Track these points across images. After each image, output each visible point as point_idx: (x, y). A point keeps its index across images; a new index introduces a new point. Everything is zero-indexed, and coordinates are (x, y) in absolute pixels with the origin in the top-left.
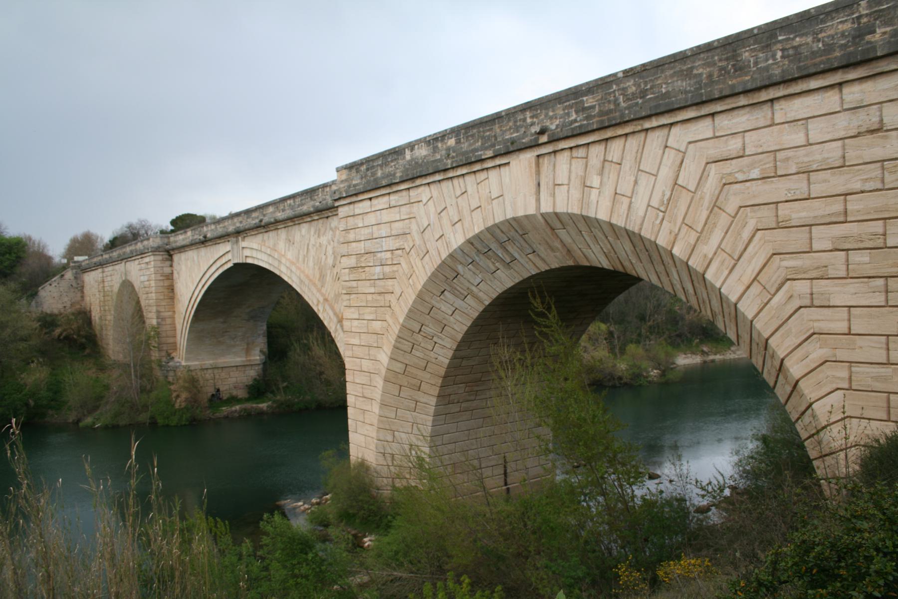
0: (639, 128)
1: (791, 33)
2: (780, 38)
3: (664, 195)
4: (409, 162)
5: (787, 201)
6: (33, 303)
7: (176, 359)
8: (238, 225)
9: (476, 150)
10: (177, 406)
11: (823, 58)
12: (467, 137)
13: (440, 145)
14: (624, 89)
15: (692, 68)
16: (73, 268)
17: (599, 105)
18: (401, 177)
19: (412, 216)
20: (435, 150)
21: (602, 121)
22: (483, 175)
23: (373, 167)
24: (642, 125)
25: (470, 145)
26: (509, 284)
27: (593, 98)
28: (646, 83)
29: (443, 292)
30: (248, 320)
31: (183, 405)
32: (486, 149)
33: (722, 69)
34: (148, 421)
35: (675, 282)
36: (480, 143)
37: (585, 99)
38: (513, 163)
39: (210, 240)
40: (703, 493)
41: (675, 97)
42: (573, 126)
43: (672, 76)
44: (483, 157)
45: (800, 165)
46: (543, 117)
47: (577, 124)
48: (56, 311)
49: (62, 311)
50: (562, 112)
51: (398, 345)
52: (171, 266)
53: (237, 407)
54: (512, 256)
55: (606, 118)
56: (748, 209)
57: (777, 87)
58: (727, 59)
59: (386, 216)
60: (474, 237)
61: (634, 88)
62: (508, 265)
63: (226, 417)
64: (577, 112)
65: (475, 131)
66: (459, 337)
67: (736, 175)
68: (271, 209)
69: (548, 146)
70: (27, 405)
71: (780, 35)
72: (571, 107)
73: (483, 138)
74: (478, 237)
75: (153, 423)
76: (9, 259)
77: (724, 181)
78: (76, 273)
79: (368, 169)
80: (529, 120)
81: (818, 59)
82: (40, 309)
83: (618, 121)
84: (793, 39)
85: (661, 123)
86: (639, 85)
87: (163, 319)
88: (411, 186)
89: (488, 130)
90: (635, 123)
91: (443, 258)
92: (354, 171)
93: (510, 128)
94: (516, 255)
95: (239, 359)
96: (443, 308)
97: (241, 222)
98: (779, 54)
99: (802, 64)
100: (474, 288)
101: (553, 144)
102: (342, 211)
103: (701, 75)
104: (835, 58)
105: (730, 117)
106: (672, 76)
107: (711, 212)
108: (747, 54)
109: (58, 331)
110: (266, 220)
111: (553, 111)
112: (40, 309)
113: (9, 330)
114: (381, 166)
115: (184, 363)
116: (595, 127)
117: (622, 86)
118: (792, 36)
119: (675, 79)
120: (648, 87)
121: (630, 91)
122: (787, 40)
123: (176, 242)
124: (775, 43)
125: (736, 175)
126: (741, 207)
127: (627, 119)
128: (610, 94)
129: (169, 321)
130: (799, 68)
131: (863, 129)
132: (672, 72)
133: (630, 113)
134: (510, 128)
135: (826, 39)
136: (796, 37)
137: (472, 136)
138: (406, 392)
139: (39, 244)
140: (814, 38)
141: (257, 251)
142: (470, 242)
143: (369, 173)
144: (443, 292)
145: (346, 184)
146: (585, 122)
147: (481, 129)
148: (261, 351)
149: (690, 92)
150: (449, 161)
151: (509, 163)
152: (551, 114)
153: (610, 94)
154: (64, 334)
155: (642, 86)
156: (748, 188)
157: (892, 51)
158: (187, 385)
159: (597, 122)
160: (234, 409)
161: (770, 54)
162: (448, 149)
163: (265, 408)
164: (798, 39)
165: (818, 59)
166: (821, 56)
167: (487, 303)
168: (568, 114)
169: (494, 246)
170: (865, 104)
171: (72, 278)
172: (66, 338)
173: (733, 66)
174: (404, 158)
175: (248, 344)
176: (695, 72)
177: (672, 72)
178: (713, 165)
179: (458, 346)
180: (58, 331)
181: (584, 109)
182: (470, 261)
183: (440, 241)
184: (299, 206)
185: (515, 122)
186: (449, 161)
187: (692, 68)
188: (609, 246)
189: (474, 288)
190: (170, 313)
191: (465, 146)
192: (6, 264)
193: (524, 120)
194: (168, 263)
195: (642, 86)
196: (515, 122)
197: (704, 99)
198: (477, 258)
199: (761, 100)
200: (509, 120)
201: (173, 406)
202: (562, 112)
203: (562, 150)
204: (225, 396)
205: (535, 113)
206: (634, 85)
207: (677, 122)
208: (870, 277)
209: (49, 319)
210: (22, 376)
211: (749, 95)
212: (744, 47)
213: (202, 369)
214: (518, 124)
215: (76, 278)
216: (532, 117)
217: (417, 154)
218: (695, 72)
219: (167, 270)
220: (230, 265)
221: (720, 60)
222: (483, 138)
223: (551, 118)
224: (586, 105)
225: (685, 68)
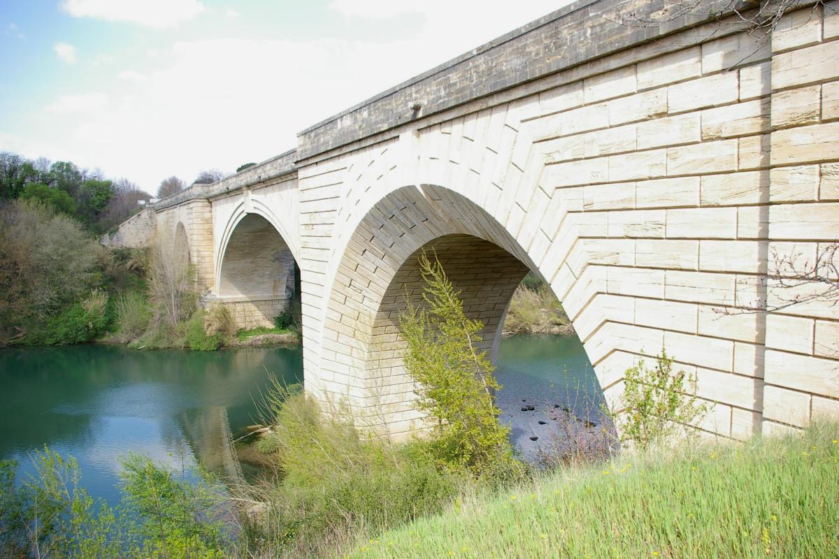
1: (600, 10)
2: (591, 15)
5: (592, 185)
6: (115, 238)
7: (213, 293)
8: (249, 179)
10: (208, 333)
11: (618, 36)
14: (476, 67)
15: (525, 46)
16: (150, 208)
18: (332, 145)
25: (377, 117)
29: (365, 251)
30: (274, 261)
31: (214, 333)
33: (547, 47)
34: (183, 345)
37: (451, 75)
38: (401, 136)
39: (232, 191)
41: (508, 75)
42: (439, 102)
43: (511, 54)
45: (602, 148)
47: (441, 101)
48: (133, 246)
49: (139, 245)
50: (435, 88)
51: (333, 296)
52: (211, 212)
53: (261, 337)
54: (412, 223)
55: (460, 95)
57: (585, 66)
58: (551, 37)
63: (251, 345)
65: (380, 104)
66: (383, 292)
67: (554, 155)
68: (269, 167)
69: (424, 120)
70: (87, 326)
71: (591, 12)
73: (384, 111)
75: (187, 348)
76: (99, 199)
78: (151, 213)
81: (614, 38)
82: (120, 243)
84: (601, 16)
85: (500, 102)
87: (203, 257)
88: (340, 153)
92: (307, 136)
95: (267, 295)
96: (367, 266)
97: (251, 177)
98: (589, 31)
99: (601, 42)
102: (301, 174)
103: (530, 52)
104: (627, 36)
105: (507, 95)
106: (511, 54)
107: (534, 191)
108: (565, 31)
109: (130, 263)
110: (264, 176)
111: (430, 87)
112: (120, 243)
113: (74, 264)
115: (218, 296)
118: (600, 13)
119: (513, 57)
122: (597, 16)
123: (213, 191)
124: (587, 20)
129: (207, 259)
130: (599, 47)
131: (652, 113)
132: (510, 49)
135: (625, 16)
136: (602, 14)
138: (343, 339)
139: (134, 186)
140: (617, 15)
141: (253, 203)
144: (365, 251)
146: (446, 99)
147: (384, 103)
148: (287, 287)
150: (361, 132)
151: (398, 136)
153: (467, 71)
154: (134, 266)
155: (490, 63)
157: (671, 30)
158: (218, 315)
160: (258, 338)
161: (582, 31)
163: (285, 339)
164: (604, 16)
165: (614, 38)
166: (616, 34)
170: (654, 85)
171: (148, 218)
172: (137, 269)
173: (555, 43)
175: (275, 282)
176: (528, 50)
177: (510, 49)
180: (130, 263)
185: (405, 97)
186: (361, 132)
187: (525, 46)
189: (389, 249)
190: (209, 253)
192: (97, 203)
194: (209, 209)
195: (490, 63)
199: (573, 79)
201: (205, 333)
202: (435, 88)
203: (435, 125)
207: (513, 101)
208: (653, 268)
209: (125, 252)
210: (85, 302)
212: (564, 25)
213: (235, 303)
214: (407, 99)
215: (150, 217)
216: (416, 92)
218: (528, 50)
219: (207, 215)
220: (244, 215)
221: (546, 38)
222: (384, 111)
225: (520, 45)
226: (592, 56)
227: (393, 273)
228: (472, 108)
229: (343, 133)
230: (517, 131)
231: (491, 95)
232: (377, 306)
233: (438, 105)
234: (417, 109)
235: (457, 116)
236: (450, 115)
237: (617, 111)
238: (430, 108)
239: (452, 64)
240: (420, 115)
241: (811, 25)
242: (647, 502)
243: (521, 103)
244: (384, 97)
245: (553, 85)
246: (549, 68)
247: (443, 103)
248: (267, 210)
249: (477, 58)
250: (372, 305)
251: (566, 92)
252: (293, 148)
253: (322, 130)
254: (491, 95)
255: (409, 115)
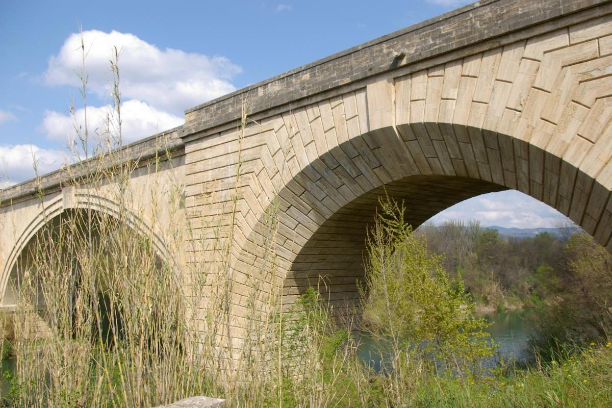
0: (497, 45)
3: (520, 97)
4: (262, 98)
9: (334, 79)
12: (322, 71)
13: (294, 80)
17: (456, 31)
18: (254, 110)
19: (262, 143)
20: (289, 85)
21: (462, 42)
22: (334, 103)
23: (224, 106)
24: (499, 42)
26: (352, 198)
27: (450, 26)
28: (502, 9)
29: (289, 208)
32: (344, 77)
35: (522, 175)
36: (335, 75)
37: (441, 28)
40: (603, 279)
42: (432, 49)
44: (340, 84)
46: (400, 46)
47: (436, 47)
56: (605, 99)
59: (231, 147)
60: (326, 154)
61: (490, 14)
62: (353, 180)
64: (433, 39)
66: (299, 249)
67: (592, 73)
72: (428, 35)
74: (331, 154)
77: (580, 79)
79: (218, 109)
80: (385, 51)
83: (477, 40)
86: (496, 11)
89: (344, 63)
90: (492, 41)
91: (294, 176)
93: (366, 59)
94: (363, 170)
100: (318, 204)
101: (410, 67)
114: (232, 104)
116: (454, 47)
117: (478, 13)
120: (505, 11)
121: (486, 17)
125: (592, 73)
126: (597, 99)
127: (487, 37)
128: (466, 21)
133: (489, 32)
134: (366, 59)
137: (327, 69)
142: (322, 159)
143: (219, 112)
145: (195, 123)
146: (444, 44)
149: (548, 9)
152: (407, 43)
156: (604, 82)
159: (456, 43)
162: (303, 82)
167: (328, 217)
168: (425, 42)
169: (343, 162)
174: (257, 94)
178: (569, 67)
179: (297, 258)
181: (441, 36)
182: (320, 177)
183: (291, 161)
184: (137, 153)
185: (372, 53)
188: (458, 152)
189: (318, 204)
191: (320, 78)
193: (381, 51)
195: (499, 12)
196: (372, 53)
197: (562, 13)
198: (326, 174)
200: (365, 52)
202: (419, 41)
203: (418, 71)
204: (409, 76)
205: (391, 44)
206: (491, 12)
211: (604, 7)
214: (374, 55)
217: (270, 91)
223: (408, 47)
224: (442, 33)
226: (537, 21)
227: (315, 228)
228: (575, 20)
229: (268, 97)
230: (539, 61)
231: (506, 35)
232: (289, 265)
233: (431, 51)
234: (401, 57)
235: (455, 58)
236: (428, 63)
237: (220, 150)
238: (420, 55)
239: (445, 17)
240: (404, 62)
241: (441, 71)
242: (42, 279)
243: (544, 38)
244: (336, 59)
245: (590, 17)
246: (545, 17)
247: (439, 49)
248: (54, 210)
249: (480, 9)
250: (284, 268)
251: (603, 22)
252: (57, 169)
253: (231, 101)
254: (506, 35)
255: (386, 65)
